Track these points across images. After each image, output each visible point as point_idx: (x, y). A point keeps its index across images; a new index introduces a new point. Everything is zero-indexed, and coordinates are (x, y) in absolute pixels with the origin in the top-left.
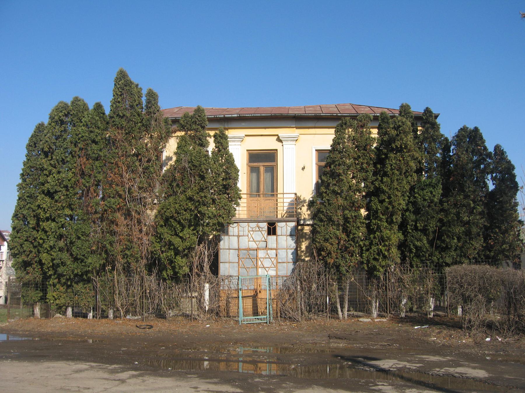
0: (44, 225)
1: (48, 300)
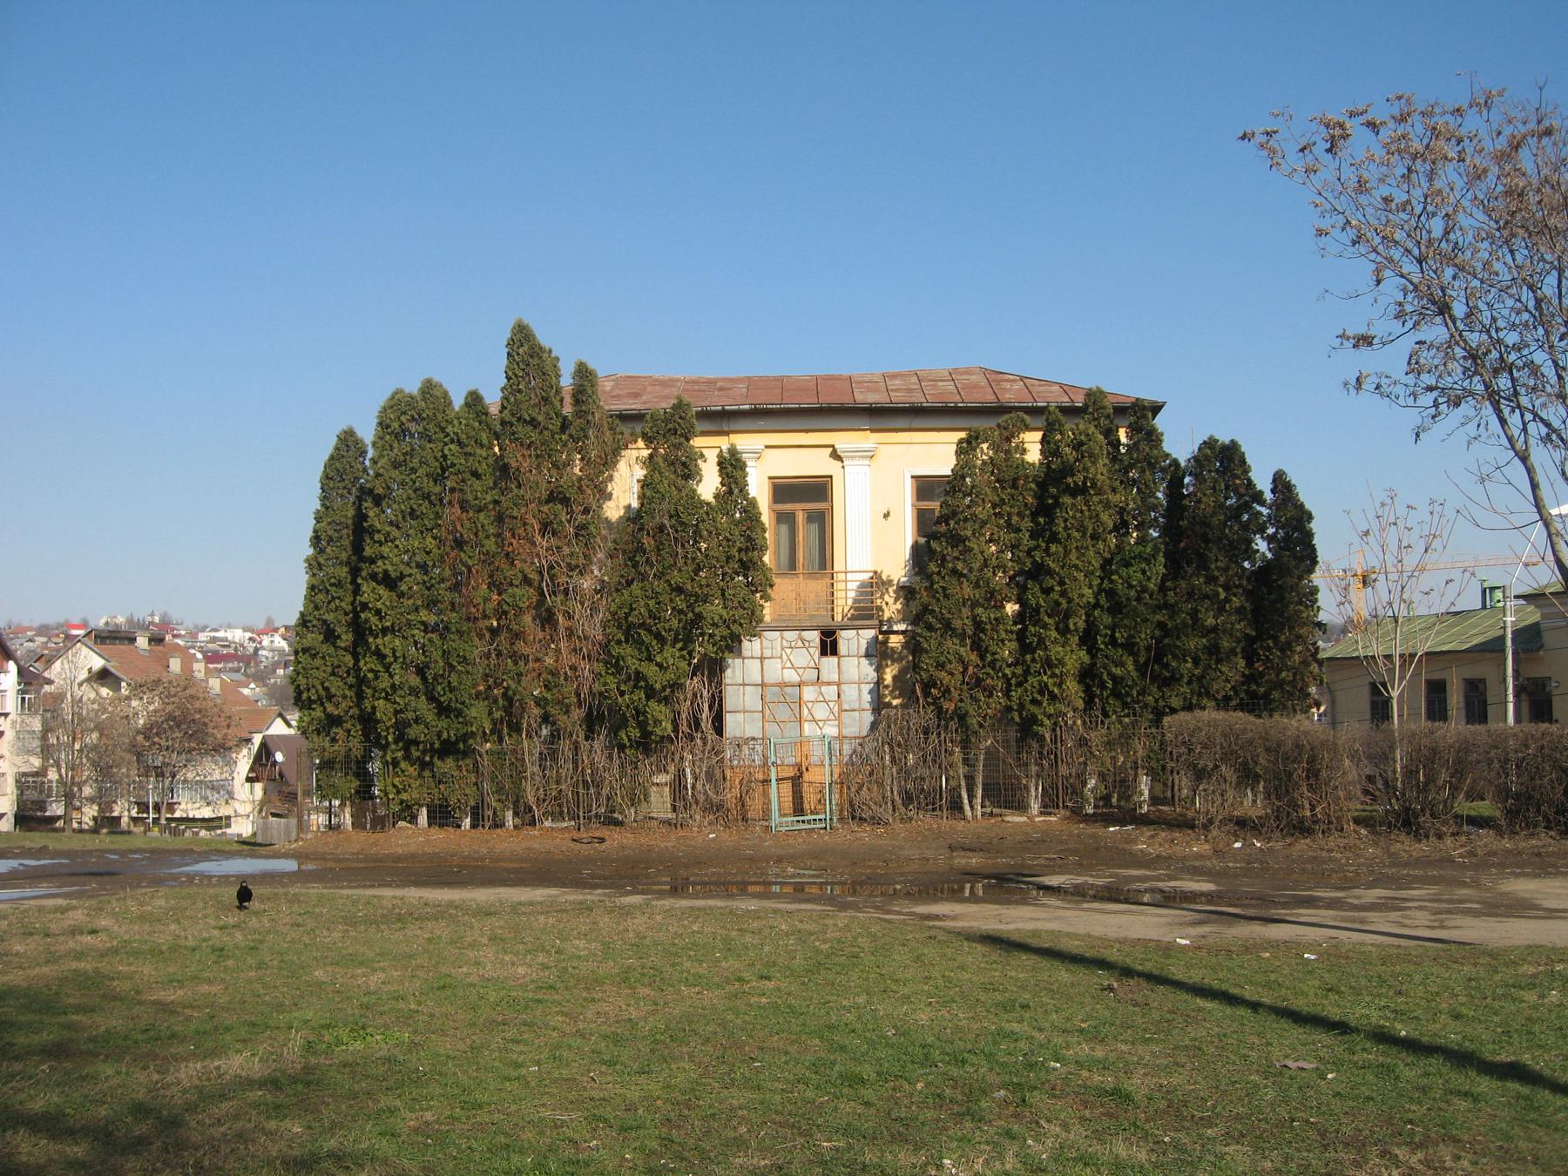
0: (386, 643)
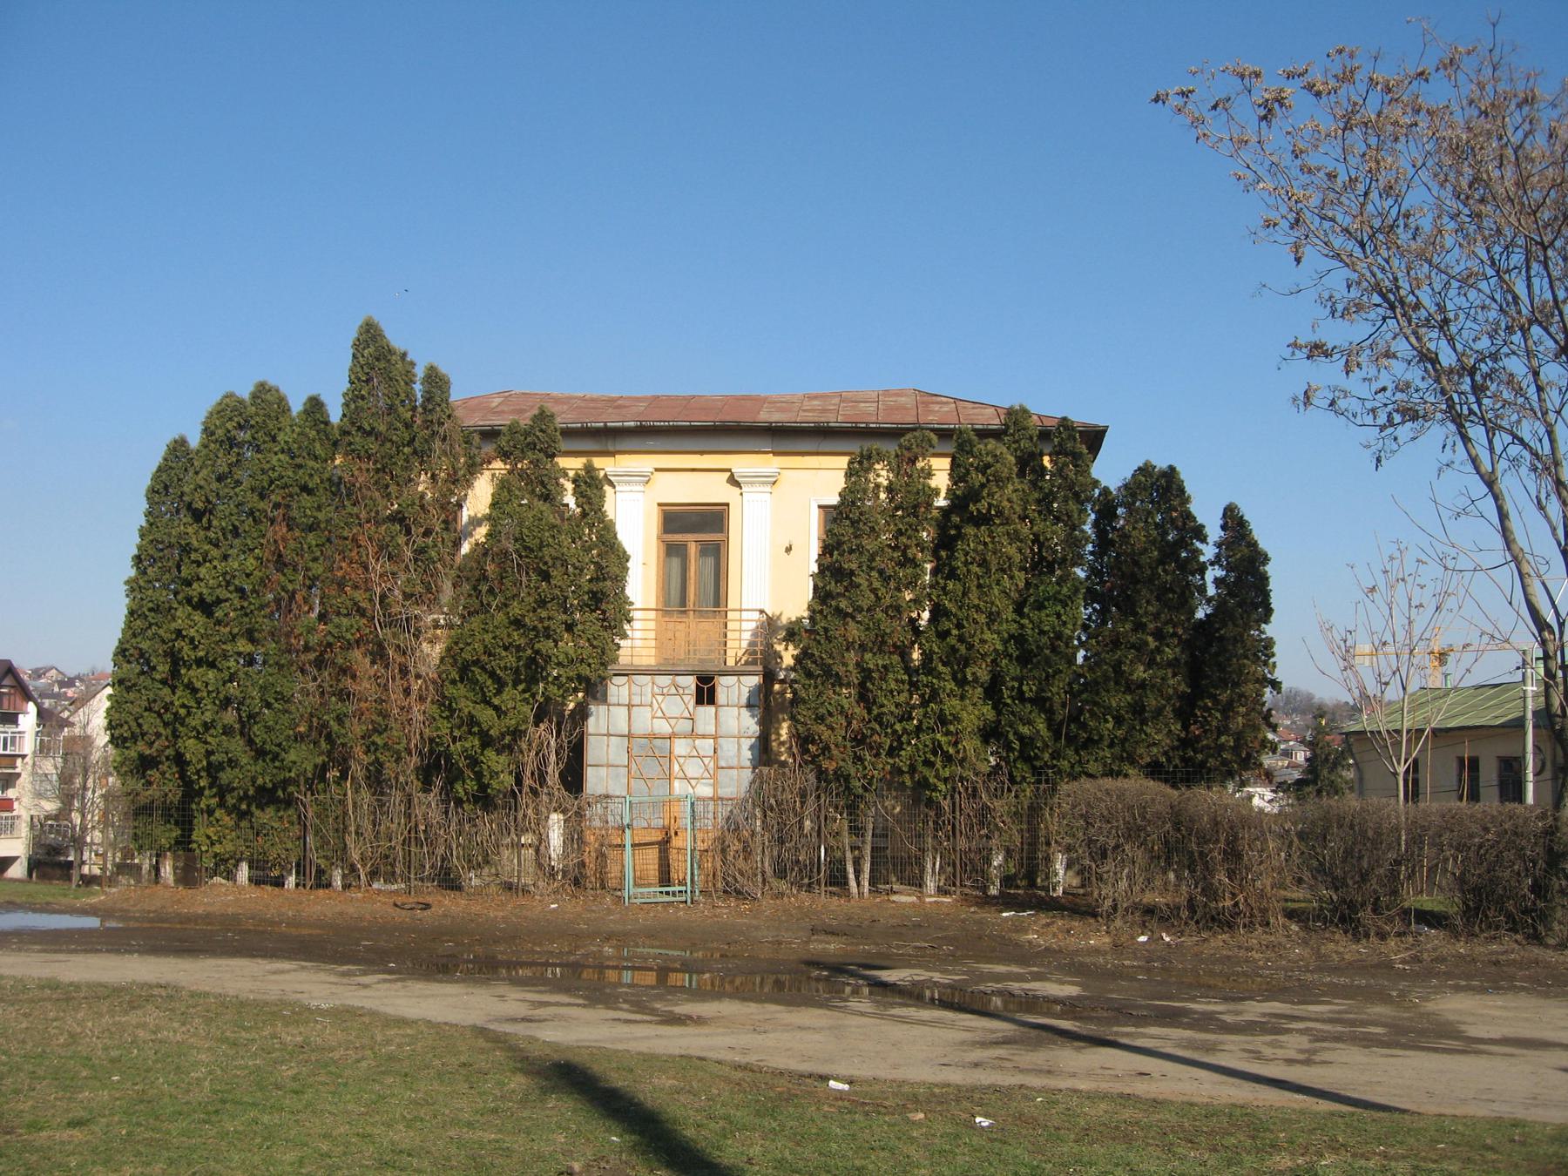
0: (194, 675)
1: (194, 846)
